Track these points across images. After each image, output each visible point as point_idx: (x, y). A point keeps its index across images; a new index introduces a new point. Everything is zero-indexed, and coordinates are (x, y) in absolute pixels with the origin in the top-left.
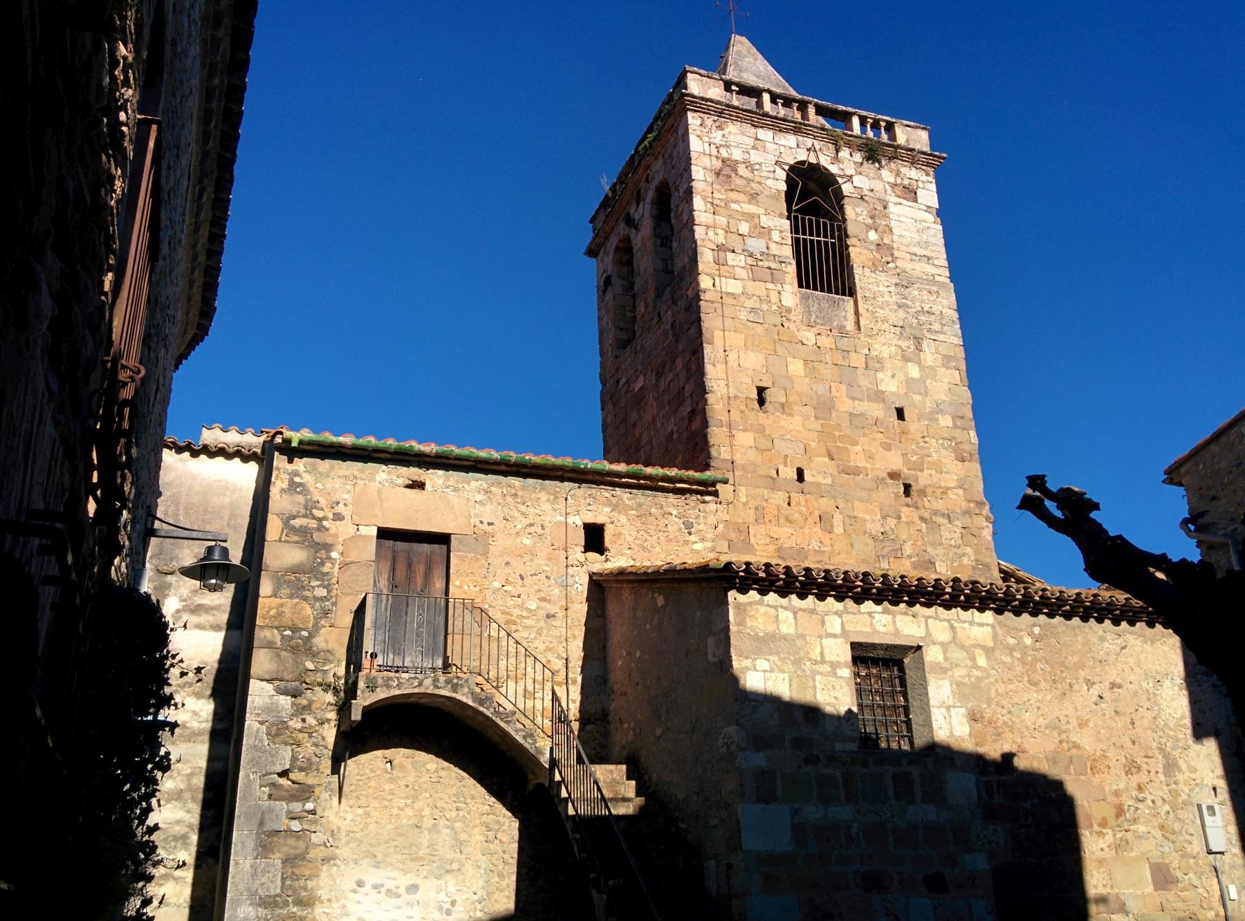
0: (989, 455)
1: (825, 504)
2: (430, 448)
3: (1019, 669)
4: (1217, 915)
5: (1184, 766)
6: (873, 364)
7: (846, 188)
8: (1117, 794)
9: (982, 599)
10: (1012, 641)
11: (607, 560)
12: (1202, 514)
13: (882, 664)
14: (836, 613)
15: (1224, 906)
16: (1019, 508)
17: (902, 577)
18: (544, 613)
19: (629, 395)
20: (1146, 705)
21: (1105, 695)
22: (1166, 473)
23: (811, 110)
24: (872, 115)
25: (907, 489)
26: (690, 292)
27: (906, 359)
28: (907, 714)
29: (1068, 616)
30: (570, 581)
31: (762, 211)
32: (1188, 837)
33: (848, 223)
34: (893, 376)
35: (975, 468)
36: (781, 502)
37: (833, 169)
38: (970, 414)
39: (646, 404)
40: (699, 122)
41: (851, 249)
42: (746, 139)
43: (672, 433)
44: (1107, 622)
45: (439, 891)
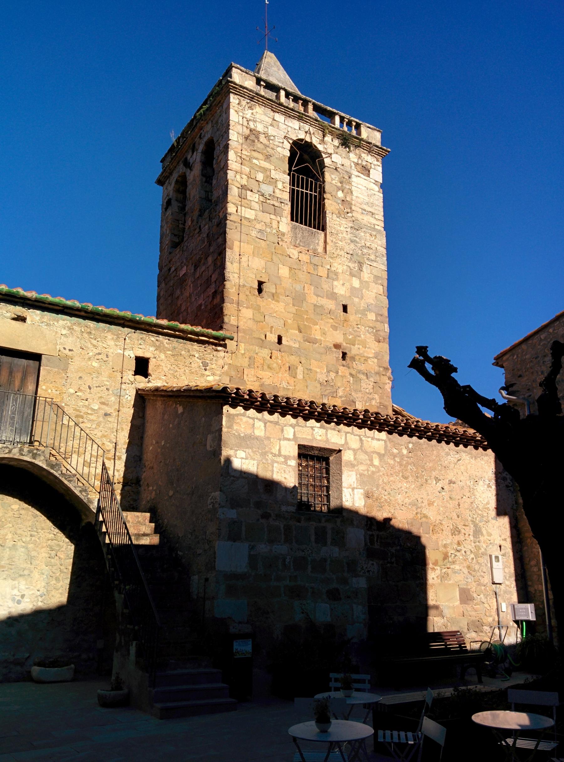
0: (394, 340)
1: (293, 360)
2: (32, 294)
3: (397, 468)
4: (494, 620)
5: (484, 532)
6: (332, 275)
7: (327, 161)
8: (445, 546)
9: (381, 425)
10: (395, 451)
11: (149, 382)
12: (512, 385)
13: (316, 458)
14: (291, 425)
15: (498, 615)
16: (409, 366)
17: (334, 406)
18: (103, 412)
19: (176, 278)
20: (468, 494)
21: (445, 488)
22: (495, 359)
23: (310, 107)
24: (348, 117)
25: (344, 355)
26: (221, 214)
27: (352, 275)
28: (328, 491)
29: (430, 439)
30: (123, 393)
31: (272, 167)
32: (482, 574)
33: (326, 184)
34: (343, 284)
35: (386, 346)
36: (266, 356)
37: (320, 147)
38: (386, 314)
39: (186, 285)
40: (237, 102)
41: (326, 201)
42: (267, 118)
43: (201, 305)
44: (452, 444)
45: (13, 588)
